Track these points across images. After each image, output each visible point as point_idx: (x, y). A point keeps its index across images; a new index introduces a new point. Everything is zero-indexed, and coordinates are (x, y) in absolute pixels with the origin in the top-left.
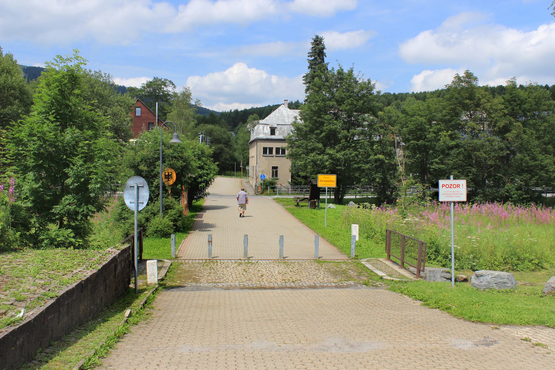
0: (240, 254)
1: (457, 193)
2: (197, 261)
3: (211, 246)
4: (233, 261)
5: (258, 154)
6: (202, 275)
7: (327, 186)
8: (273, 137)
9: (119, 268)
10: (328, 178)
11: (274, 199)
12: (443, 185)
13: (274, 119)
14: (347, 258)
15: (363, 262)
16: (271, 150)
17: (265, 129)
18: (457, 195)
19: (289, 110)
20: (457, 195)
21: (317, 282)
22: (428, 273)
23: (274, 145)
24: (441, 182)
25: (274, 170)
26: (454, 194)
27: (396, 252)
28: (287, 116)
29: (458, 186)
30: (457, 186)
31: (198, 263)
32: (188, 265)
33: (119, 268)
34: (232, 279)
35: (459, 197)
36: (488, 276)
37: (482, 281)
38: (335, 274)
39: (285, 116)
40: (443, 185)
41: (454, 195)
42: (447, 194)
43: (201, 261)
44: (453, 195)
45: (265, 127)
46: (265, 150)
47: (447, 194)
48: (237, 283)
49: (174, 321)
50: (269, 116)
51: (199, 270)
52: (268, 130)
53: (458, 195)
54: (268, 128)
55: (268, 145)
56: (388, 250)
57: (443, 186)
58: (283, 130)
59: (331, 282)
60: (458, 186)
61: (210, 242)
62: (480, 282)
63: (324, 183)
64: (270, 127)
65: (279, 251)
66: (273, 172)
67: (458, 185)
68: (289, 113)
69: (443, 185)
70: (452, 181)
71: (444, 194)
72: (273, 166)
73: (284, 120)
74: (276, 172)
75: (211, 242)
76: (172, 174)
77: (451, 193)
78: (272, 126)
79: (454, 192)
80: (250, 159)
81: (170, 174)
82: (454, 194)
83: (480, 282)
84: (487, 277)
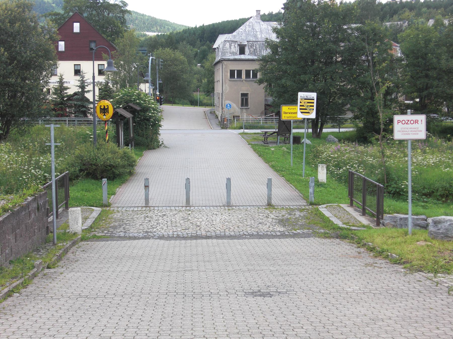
0: (224, 200)
1: (414, 130)
2: (132, 209)
3: (147, 191)
4: (173, 208)
5: (223, 78)
6: (134, 224)
7: (292, 118)
8: (242, 57)
9: (33, 217)
10: (293, 109)
11: (240, 134)
12: (399, 121)
13: (244, 35)
14: (305, 204)
15: (323, 209)
16: (239, 72)
17: (232, 47)
18: (415, 132)
19: (262, 23)
20: (415, 132)
21: (261, 231)
22: (398, 221)
23: (244, 67)
24: (397, 118)
25: (244, 98)
26: (411, 131)
27: (358, 199)
28: (260, 30)
29: (416, 122)
30: (416, 122)
31: (133, 211)
32: (120, 214)
33: (33, 217)
34: (166, 228)
35: (418, 134)
36: (447, 223)
37: (439, 228)
38: (282, 222)
39: (257, 30)
40: (399, 122)
41: (412, 132)
42: (403, 131)
43: (136, 209)
44: (411, 132)
45: (233, 44)
46: (232, 72)
47: (403, 131)
48: (171, 233)
49: (87, 272)
50: (237, 31)
51: (132, 219)
52: (234, 48)
53: (416, 132)
54: (236, 46)
55: (236, 67)
56: (351, 194)
57: (398, 122)
58: (254, 48)
59: (276, 231)
60: (416, 122)
61: (147, 187)
62: (438, 229)
63: (288, 115)
64: (239, 45)
65: (267, 198)
66: (242, 100)
67: (417, 121)
68: (261, 26)
69: (399, 121)
70: (409, 117)
71: (400, 131)
72: (242, 92)
73: (255, 36)
74: (247, 100)
75: (148, 186)
76: (108, 108)
77: (407, 130)
78: (241, 43)
79: (411, 128)
80: (215, 84)
81: (106, 107)
82: (411, 131)
83: (438, 229)
84: (445, 224)
